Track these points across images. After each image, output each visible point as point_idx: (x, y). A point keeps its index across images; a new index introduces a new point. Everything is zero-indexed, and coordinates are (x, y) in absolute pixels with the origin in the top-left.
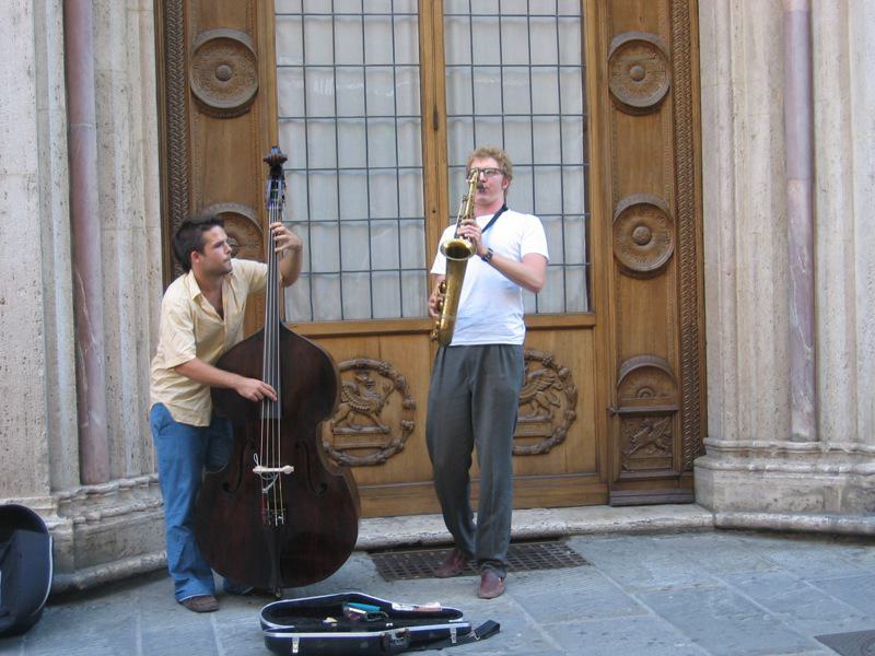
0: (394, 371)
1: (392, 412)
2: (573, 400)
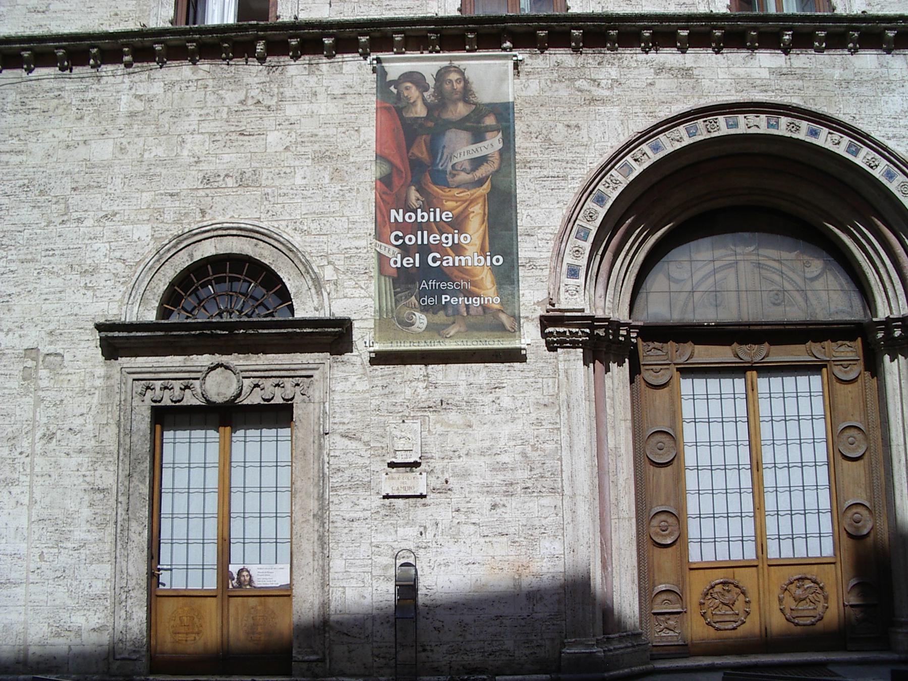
0: (740, 585)
1: (739, 605)
2: (826, 599)
